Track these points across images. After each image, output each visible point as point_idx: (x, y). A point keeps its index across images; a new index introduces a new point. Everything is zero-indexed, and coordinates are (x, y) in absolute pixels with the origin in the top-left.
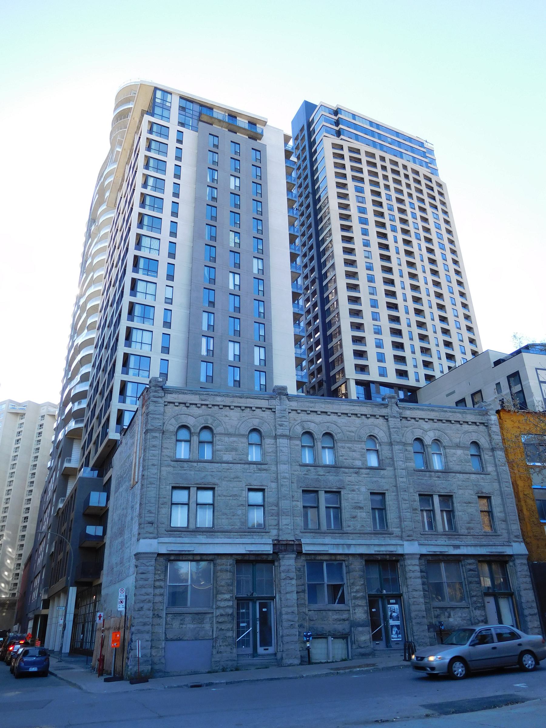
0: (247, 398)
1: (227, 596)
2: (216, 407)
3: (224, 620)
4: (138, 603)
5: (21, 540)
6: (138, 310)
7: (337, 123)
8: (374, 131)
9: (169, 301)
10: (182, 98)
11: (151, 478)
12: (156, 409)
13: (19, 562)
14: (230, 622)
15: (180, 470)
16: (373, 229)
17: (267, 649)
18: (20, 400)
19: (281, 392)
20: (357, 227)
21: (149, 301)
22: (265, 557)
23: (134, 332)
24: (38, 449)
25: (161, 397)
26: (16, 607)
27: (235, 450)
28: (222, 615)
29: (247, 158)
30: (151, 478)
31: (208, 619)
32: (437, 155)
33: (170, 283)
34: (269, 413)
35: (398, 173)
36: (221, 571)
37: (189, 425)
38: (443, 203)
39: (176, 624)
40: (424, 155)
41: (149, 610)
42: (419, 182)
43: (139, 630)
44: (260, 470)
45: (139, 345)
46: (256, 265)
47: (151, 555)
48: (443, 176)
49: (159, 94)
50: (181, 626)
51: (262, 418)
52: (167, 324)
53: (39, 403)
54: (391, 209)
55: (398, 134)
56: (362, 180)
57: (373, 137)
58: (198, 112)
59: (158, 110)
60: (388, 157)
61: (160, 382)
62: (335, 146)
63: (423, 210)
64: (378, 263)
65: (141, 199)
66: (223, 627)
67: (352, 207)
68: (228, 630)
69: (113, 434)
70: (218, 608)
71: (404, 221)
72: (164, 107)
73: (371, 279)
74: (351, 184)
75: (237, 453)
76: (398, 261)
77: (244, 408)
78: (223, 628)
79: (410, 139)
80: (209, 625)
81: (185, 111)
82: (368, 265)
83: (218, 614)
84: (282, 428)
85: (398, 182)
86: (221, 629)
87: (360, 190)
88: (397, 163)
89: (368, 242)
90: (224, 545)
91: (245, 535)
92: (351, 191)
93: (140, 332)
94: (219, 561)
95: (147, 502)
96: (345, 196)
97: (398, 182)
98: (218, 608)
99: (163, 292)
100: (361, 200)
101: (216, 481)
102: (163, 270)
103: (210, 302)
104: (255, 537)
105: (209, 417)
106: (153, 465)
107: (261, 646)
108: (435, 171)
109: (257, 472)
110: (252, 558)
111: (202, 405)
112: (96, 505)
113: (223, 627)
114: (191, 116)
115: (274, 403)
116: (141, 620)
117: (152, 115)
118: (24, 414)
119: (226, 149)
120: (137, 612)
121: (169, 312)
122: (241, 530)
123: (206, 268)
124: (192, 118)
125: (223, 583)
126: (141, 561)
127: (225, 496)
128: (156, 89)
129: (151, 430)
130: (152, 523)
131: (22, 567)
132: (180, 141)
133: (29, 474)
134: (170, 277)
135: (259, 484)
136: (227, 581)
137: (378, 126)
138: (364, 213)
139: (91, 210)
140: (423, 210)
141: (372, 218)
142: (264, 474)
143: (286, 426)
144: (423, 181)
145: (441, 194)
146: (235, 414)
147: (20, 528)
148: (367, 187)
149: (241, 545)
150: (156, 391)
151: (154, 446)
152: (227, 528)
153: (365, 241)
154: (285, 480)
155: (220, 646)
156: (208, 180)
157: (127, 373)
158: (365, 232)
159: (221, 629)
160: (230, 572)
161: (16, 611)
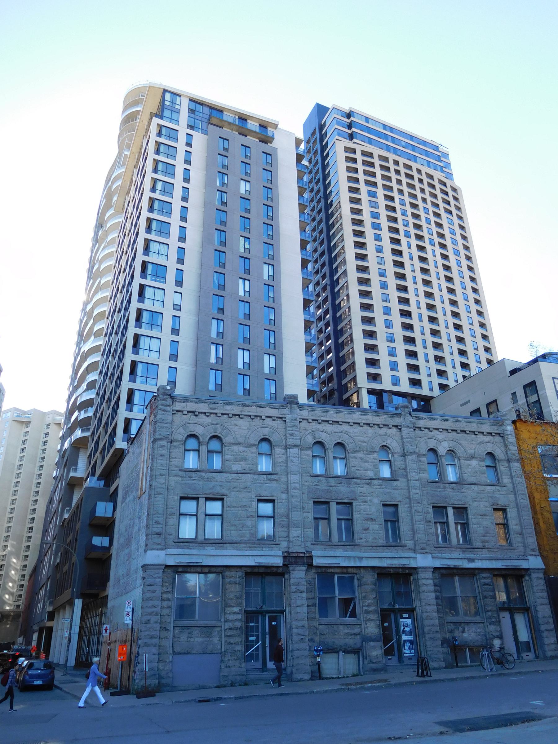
0: (257, 406)
1: (236, 609)
2: (225, 416)
6: (145, 317)
7: (350, 126)
8: (388, 135)
9: (178, 307)
10: (191, 100)
13: (23, 573)
14: (239, 636)
15: (188, 480)
16: (386, 235)
18: (26, 409)
23: (142, 339)
24: (43, 458)
25: (169, 406)
28: (230, 629)
31: (217, 632)
32: (453, 159)
33: (178, 289)
34: (279, 422)
36: (230, 583)
38: (458, 209)
39: (184, 637)
40: (439, 159)
44: (270, 480)
45: (146, 353)
46: (267, 271)
47: (157, 567)
48: (458, 181)
49: (168, 96)
50: (189, 639)
52: (175, 331)
53: (45, 411)
54: (404, 214)
55: (412, 137)
56: (375, 184)
57: (387, 140)
58: (208, 115)
59: (167, 113)
60: (402, 160)
62: (347, 149)
63: (437, 215)
64: (391, 270)
66: (232, 640)
67: (364, 212)
68: (237, 644)
69: (120, 443)
71: (418, 227)
74: (364, 188)
75: (246, 463)
76: (412, 267)
78: (232, 642)
79: (425, 143)
82: (381, 271)
83: (227, 627)
84: (292, 437)
85: (412, 187)
87: (373, 195)
92: (364, 195)
94: (227, 573)
97: (412, 187)
98: (227, 621)
99: (172, 298)
100: (374, 205)
101: (224, 491)
102: (171, 276)
105: (218, 426)
106: (161, 475)
108: (450, 176)
113: (232, 640)
114: (200, 119)
115: (285, 412)
116: (148, 633)
118: (30, 422)
120: (145, 625)
123: (215, 274)
124: (202, 121)
127: (234, 507)
128: (165, 91)
129: (159, 439)
130: (159, 534)
131: (27, 578)
132: (189, 144)
134: (179, 283)
135: (269, 495)
137: (392, 129)
140: (437, 215)
141: (385, 224)
142: (274, 485)
144: (438, 186)
146: (244, 423)
147: (25, 539)
148: (381, 192)
149: (251, 557)
150: (163, 400)
151: (161, 456)
154: (296, 491)
155: (229, 660)
156: (218, 184)
158: (378, 238)
160: (239, 584)
161: (20, 623)
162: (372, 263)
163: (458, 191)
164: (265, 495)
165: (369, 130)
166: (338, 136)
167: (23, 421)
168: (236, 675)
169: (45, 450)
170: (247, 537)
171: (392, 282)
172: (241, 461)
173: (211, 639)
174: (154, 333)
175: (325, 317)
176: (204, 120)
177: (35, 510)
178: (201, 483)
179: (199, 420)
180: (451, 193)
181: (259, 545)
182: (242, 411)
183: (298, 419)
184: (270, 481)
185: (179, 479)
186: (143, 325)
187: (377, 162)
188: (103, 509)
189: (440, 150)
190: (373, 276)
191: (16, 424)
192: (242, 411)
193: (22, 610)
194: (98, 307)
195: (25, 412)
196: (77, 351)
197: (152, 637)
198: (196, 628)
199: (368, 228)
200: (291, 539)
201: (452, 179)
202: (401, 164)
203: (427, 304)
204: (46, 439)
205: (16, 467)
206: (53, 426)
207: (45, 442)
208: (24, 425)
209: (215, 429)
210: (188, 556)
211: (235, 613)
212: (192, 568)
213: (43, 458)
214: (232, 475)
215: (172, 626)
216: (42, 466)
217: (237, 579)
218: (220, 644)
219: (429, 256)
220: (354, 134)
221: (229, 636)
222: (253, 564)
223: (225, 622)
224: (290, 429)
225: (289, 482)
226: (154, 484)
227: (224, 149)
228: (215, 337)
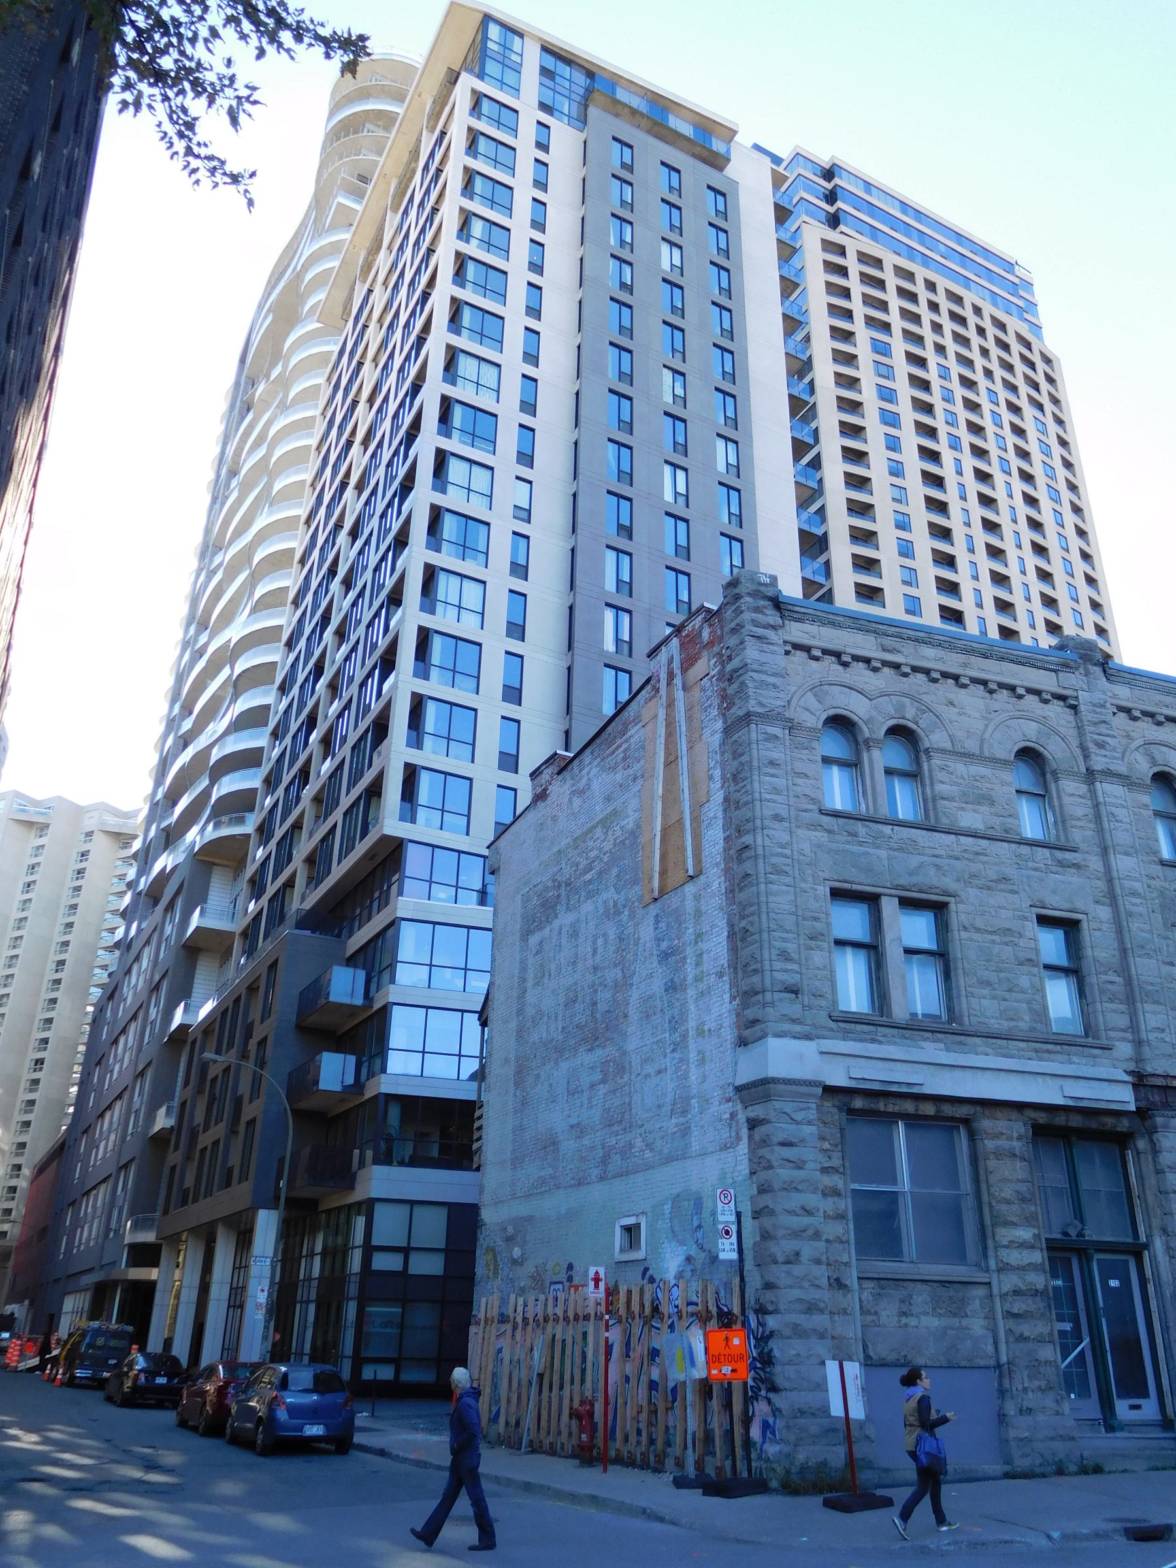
0: (1002, 659)
1: (1025, 1234)
2: (919, 676)
3: (1024, 1307)
4: (784, 1237)
5: (26, 1112)
6: (449, 526)
7: (831, 197)
8: (910, 222)
9: (524, 514)
10: (547, 49)
11: (777, 855)
12: (764, 658)
13: (17, 1161)
14: (1042, 1315)
15: (848, 843)
16: (911, 441)
17: (1137, 1407)
18: (38, 796)
19: (1086, 655)
20: (875, 432)
21: (476, 507)
22: (1109, 1121)
23: (442, 578)
24: (74, 907)
25: (774, 627)
26: (11, 1264)
27: (988, 800)
28: (1017, 1292)
29: (699, 208)
30: (777, 855)
31: (977, 1303)
32: (1040, 295)
33: (525, 472)
34: (1059, 709)
35: (962, 321)
36: (998, 1154)
37: (855, 718)
38: (1056, 401)
39: (888, 1313)
40: (1014, 288)
41: (818, 1262)
42: (1005, 347)
43: (796, 1325)
44: (1061, 864)
45: (452, 612)
46: (722, 454)
47: (804, 1089)
48: (1052, 340)
49: (494, 31)
50: (904, 1320)
51: (1042, 721)
52: (520, 570)
53: (82, 804)
54: (948, 399)
55: (959, 237)
56: (886, 327)
57: (909, 237)
58: (582, 85)
59: (492, 68)
60: (942, 283)
61: (765, 585)
62: (828, 245)
63: (1015, 409)
64: (921, 517)
65: (455, 263)
66: (1026, 1329)
67: (864, 384)
68: (1040, 1340)
69: (391, 823)
70: (1003, 1268)
71: (976, 429)
72: (507, 62)
73: (906, 550)
74: (863, 334)
75: (993, 810)
76: (964, 516)
77: (995, 687)
78: (1026, 1334)
79: (986, 252)
80: (982, 1322)
81: (553, 79)
82: (900, 517)
83: (1006, 1287)
84: (1103, 752)
85: (964, 341)
86: (1021, 1335)
87: (882, 349)
88: (961, 298)
89: (900, 466)
90: (1003, 1074)
91: (1048, 1051)
92: (862, 347)
93: (454, 581)
94: (986, 1124)
95: (773, 926)
96: (850, 359)
97: (964, 341)
98: (1003, 1268)
99: (511, 494)
100: (885, 371)
101: (948, 883)
102: (508, 440)
103: (620, 527)
104: (1075, 1059)
105: (907, 701)
106: (777, 818)
107: (1119, 1397)
108: (1036, 328)
109: (1054, 869)
110: (1076, 1121)
111: (885, 663)
112: (346, 1000)
113: (1026, 1329)
114: (566, 93)
115: (1071, 681)
116: (796, 1293)
117: (481, 76)
118: (47, 826)
119: (652, 182)
120: (784, 1268)
121: (523, 541)
122: (1033, 1035)
123: (611, 445)
124: (569, 98)
125: (1007, 1192)
126: (777, 1105)
127: (978, 930)
128: (487, 18)
129: (759, 715)
130: (794, 991)
131: (26, 1172)
132: (543, 146)
133: (50, 961)
134: (526, 458)
135: (1066, 906)
136: (1019, 1187)
137: (919, 214)
138: (891, 402)
139: (243, 361)
140: (1015, 409)
141: (908, 416)
142: (1072, 878)
143: (1114, 750)
144: (1016, 347)
145: (1051, 380)
146: (972, 699)
147: (24, 1084)
148: (899, 346)
149: (1048, 1078)
150: (757, 610)
151: (772, 763)
152: (996, 1025)
153: (894, 464)
154: (1138, 901)
155: (1025, 1390)
156: (612, 242)
157: (426, 677)
158: (893, 444)
159: (1021, 1335)
160: (1023, 1159)
161: (10, 1271)
162: (880, 496)
163: (1055, 363)
164: (1055, 905)
165: (872, 209)
166: (807, 214)
167: (33, 823)
168: (1052, 1439)
169: (78, 889)
170: (1024, 1024)
171: (924, 544)
172: (979, 803)
173: (965, 1322)
174: (469, 567)
176: (574, 96)
177: (49, 1021)
178: (883, 853)
179: (857, 678)
180: (1040, 365)
181: (1058, 1048)
182: (965, 665)
183: (1108, 705)
184: (1063, 866)
185: (822, 836)
186: (445, 545)
187: (892, 281)
188: (344, 985)
189: (1017, 273)
190: (883, 525)
192: (965, 665)
193: (14, 1244)
194: (267, 542)
197: (811, 1308)
198: (919, 1286)
199: (871, 420)
200: (1144, 1036)
201: (1040, 337)
202: (940, 290)
203: (996, 599)
204: (81, 866)
205: (11, 923)
206: (99, 838)
207: (80, 872)
208: (34, 832)
209: (900, 708)
210: (880, 1064)
211: (1023, 1245)
212: (892, 1100)
213: (74, 907)
214: (963, 839)
215: (855, 1274)
216: (70, 925)
217: (1016, 1144)
218: (991, 1341)
219: (999, 494)
220: (841, 214)
221: (1016, 1316)
222: (1059, 1101)
223: (999, 1270)
224: (1092, 728)
225: (1115, 874)
226: (759, 841)
227: (624, 165)
228: (614, 590)
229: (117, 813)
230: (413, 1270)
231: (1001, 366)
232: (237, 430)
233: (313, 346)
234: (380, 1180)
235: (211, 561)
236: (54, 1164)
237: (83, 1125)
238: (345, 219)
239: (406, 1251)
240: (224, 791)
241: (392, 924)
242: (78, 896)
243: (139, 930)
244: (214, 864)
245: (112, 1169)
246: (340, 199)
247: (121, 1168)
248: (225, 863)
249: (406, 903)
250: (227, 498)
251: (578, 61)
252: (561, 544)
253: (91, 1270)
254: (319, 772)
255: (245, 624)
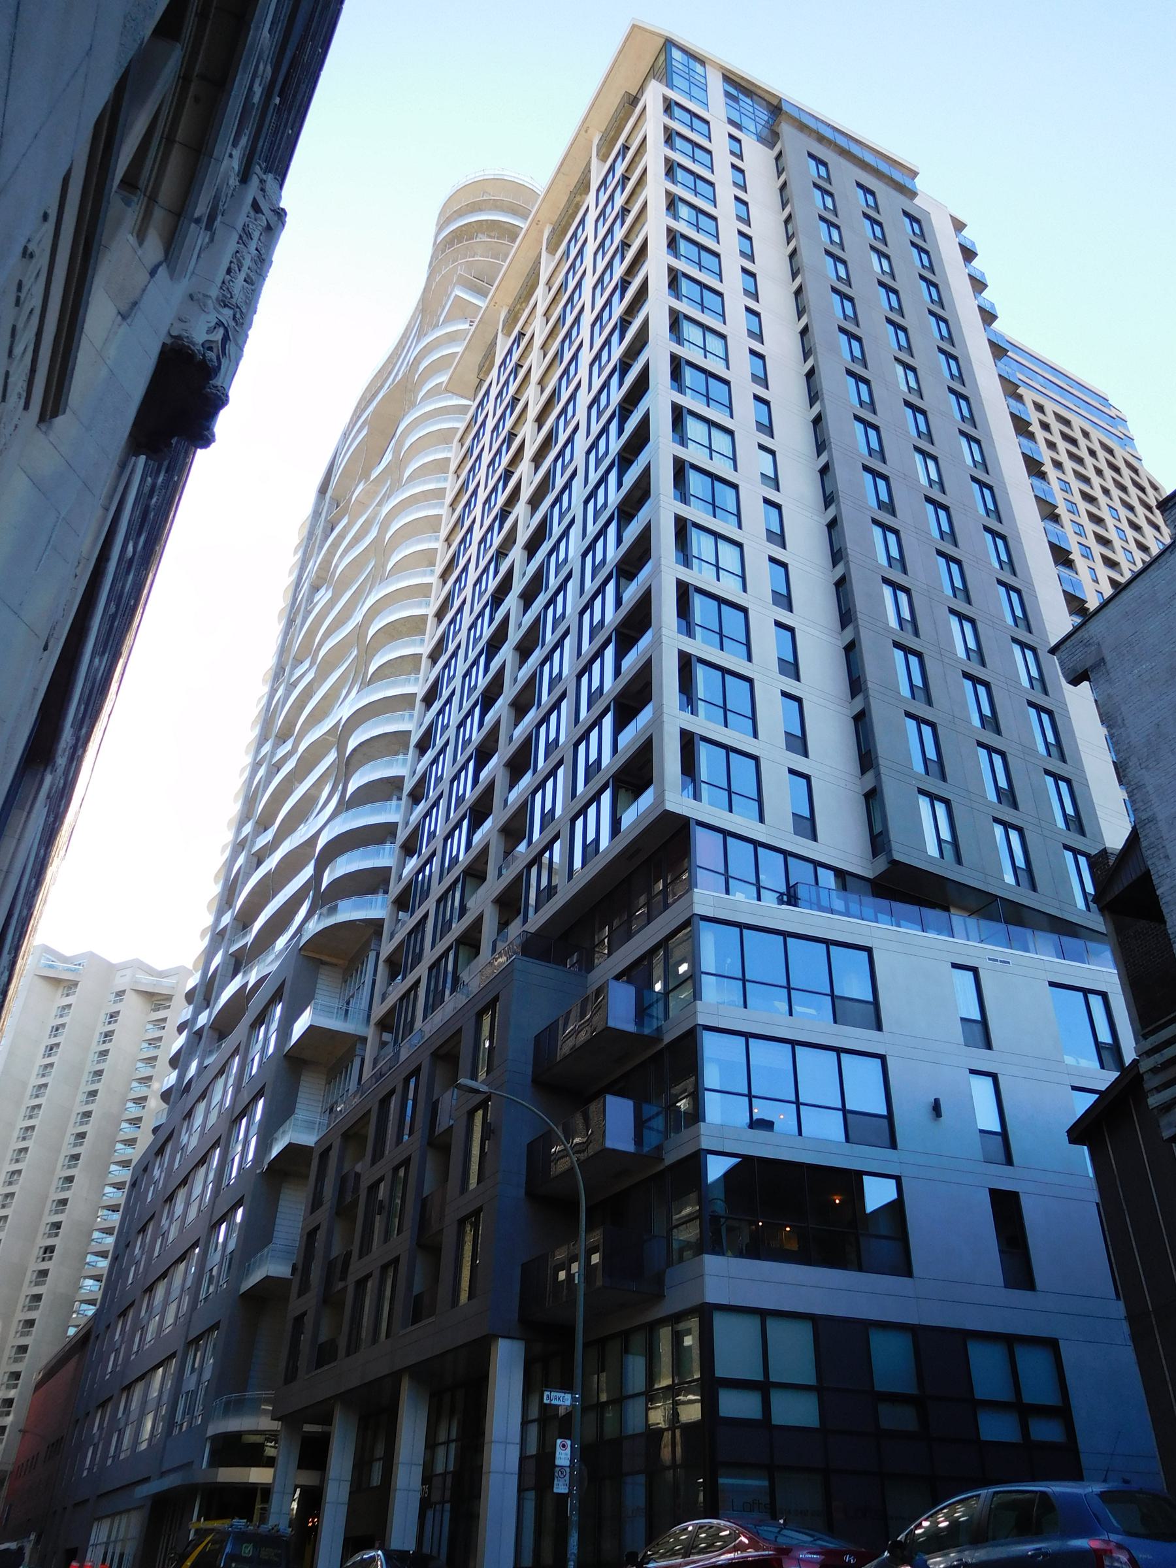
18: (68, 953)
24: (99, 1073)
117: (670, 85)
118: (76, 984)
128: (669, 43)
147: (30, 1276)
169: (104, 1053)
175: (508, 852)
177: (64, 1202)
191: (38, 981)
195: (65, 959)
196: (612, 133)
205: (29, 1090)
206: (130, 997)
207: (108, 1035)
213: (99, 1073)
216: (93, 1093)
229: (150, 971)
230: (778, 1419)
231: (1084, 499)
232: (321, 548)
233: (438, 416)
234: (724, 1277)
235: (291, 674)
236: (72, 1363)
237: (120, 1302)
238: (462, 310)
239: (764, 1387)
240: (339, 873)
241: (687, 923)
242: (104, 1061)
243: (202, 1069)
244: (323, 963)
245: (179, 1346)
246: (459, 292)
247: (190, 1343)
248: (334, 960)
249: (706, 897)
250: (310, 612)
251: (759, 92)
252: (816, 518)
253: (146, 1480)
254: (506, 801)
255: (351, 705)
